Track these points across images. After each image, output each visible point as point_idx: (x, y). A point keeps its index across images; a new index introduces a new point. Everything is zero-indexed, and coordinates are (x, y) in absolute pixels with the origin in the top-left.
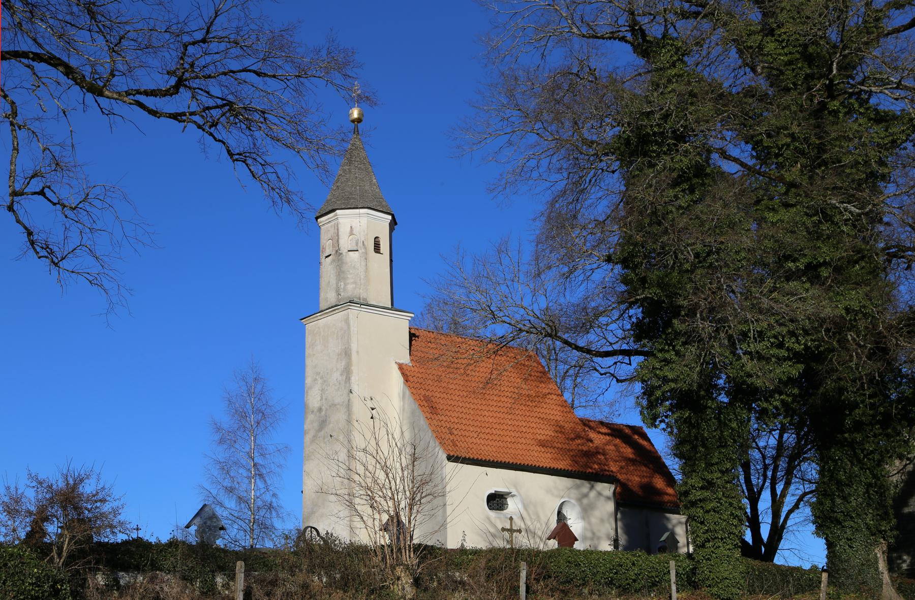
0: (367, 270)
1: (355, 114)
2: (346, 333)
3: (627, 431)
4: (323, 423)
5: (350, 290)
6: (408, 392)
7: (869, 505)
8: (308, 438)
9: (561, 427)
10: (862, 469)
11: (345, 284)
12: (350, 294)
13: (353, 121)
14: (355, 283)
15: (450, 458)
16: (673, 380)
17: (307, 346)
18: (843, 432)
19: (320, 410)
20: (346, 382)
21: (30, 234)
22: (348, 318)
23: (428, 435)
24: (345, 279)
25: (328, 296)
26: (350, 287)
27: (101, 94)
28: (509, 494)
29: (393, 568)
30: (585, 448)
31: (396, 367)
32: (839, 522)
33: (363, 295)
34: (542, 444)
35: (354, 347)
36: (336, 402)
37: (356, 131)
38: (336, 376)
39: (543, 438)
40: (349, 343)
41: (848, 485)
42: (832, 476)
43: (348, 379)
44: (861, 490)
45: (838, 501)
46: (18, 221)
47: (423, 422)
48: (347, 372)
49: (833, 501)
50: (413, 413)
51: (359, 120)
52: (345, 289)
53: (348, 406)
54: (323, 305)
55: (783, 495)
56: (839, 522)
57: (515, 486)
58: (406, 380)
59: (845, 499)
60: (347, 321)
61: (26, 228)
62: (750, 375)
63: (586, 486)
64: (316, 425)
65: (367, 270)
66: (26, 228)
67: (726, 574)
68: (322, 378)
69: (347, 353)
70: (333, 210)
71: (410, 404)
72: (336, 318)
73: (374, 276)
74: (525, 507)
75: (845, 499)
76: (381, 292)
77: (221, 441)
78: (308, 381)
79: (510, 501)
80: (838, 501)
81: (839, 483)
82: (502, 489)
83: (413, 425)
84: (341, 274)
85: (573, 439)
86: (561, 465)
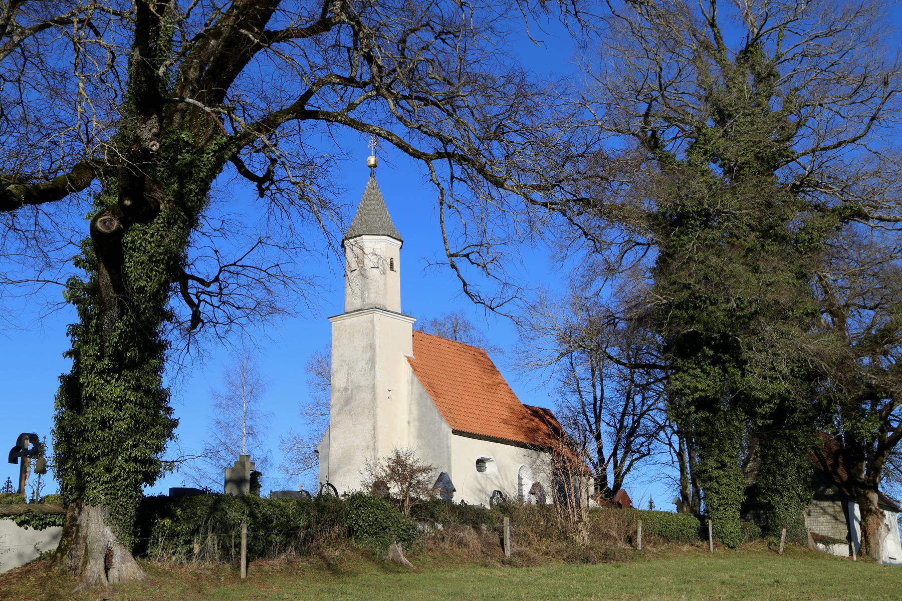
0: (385, 284)
1: (372, 160)
2: (371, 331)
3: (541, 412)
4: (348, 401)
5: (373, 298)
6: (416, 379)
7: (799, 481)
8: (333, 411)
9: (513, 409)
10: (795, 455)
11: (369, 293)
12: (372, 301)
13: (370, 166)
14: (376, 293)
15: (455, 432)
16: (701, 391)
17: (333, 338)
18: (784, 430)
19: (346, 389)
20: (371, 370)
21: (465, 284)
22: (373, 320)
23: (436, 415)
24: (368, 289)
25: (353, 301)
26: (373, 296)
27: (502, 186)
28: (488, 459)
29: (576, 523)
30: (530, 426)
31: (406, 360)
32: (778, 492)
33: (383, 303)
34: (505, 422)
35: (377, 342)
36: (362, 384)
37: (372, 174)
38: (362, 364)
39: (505, 417)
40: (374, 339)
41: (785, 466)
42: (773, 460)
43: (373, 367)
44: (794, 471)
45: (778, 478)
46: (459, 276)
47: (429, 402)
48: (372, 361)
49: (774, 477)
50: (421, 395)
51: (375, 166)
52: (368, 298)
53: (373, 388)
54: (348, 308)
55: (623, 461)
56: (778, 492)
57: (493, 454)
58: (415, 370)
59: (784, 476)
60: (372, 322)
61: (463, 281)
62: (752, 389)
63: (534, 454)
64: (342, 401)
65: (385, 284)
66: (463, 281)
67: (732, 530)
68: (348, 364)
69: (372, 347)
70: (360, 235)
71: (418, 388)
72: (362, 319)
73: (388, 288)
74: (499, 470)
75: (784, 476)
76: (394, 301)
77: (219, 406)
78: (334, 366)
79: (487, 464)
80: (778, 478)
81: (780, 465)
82: (485, 456)
83: (421, 405)
84: (364, 288)
85: (522, 419)
86: (521, 438)
